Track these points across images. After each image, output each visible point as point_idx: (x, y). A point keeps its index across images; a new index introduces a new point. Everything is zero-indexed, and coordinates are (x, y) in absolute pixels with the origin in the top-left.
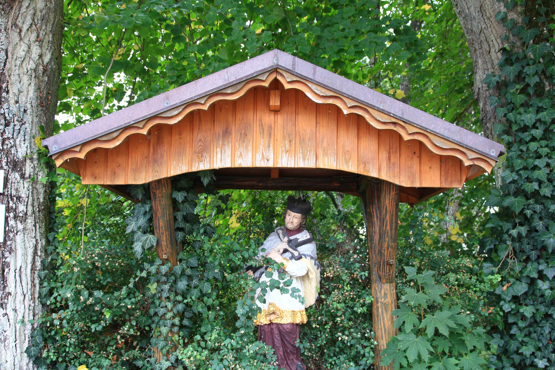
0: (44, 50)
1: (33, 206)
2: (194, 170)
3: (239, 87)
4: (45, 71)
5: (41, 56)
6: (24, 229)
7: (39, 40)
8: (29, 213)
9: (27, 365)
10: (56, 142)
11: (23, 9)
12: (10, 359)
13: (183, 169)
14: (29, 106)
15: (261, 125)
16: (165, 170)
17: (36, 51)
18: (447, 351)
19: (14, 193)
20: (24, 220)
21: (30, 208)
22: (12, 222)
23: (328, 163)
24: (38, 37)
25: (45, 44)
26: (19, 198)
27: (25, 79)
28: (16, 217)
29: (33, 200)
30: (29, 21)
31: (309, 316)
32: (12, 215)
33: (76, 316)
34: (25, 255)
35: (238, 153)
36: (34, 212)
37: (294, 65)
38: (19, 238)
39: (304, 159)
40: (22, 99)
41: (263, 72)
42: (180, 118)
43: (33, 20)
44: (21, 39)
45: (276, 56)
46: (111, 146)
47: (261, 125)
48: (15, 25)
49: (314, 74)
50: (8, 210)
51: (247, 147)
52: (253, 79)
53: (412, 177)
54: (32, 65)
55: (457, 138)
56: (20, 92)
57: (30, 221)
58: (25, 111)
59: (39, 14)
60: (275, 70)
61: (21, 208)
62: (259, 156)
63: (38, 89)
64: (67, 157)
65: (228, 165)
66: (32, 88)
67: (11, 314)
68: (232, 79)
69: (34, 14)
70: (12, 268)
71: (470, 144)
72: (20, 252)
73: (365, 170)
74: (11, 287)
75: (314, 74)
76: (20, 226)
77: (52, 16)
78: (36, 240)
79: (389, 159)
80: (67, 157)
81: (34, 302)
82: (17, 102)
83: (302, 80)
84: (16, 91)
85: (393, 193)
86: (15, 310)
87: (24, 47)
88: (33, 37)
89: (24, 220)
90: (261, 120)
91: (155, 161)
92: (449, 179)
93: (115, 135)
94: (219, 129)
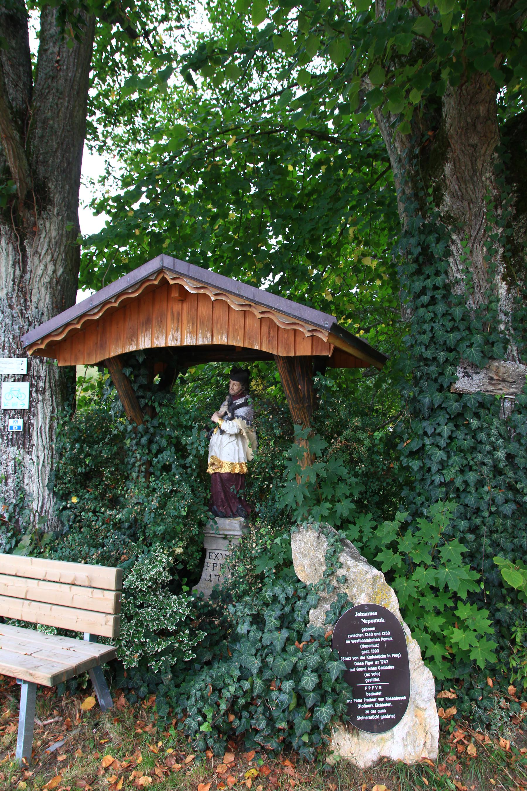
0: (57, 266)
1: (50, 382)
2: (126, 351)
3: (137, 287)
4: (57, 282)
5: (54, 272)
6: (44, 399)
7: (54, 261)
8: (47, 387)
9: (49, 495)
10: (27, 339)
11: (42, 240)
12: (35, 489)
13: (120, 351)
14: (45, 310)
15: (172, 313)
16: (107, 352)
17: (51, 268)
18: (329, 498)
19: (35, 374)
20: (43, 393)
21: (47, 384)
22: (34, 395)
23: (220, 340)
24: (53, 257)
25: (59, 262)
26: (39, 377)
27: (43, 290)
28: (37, 391)
29: (50, 378)
30: (46, 247)
31: (249, 468)
32: (34, 389)
33: (69, 462)
34: (44, 418)
35: (156, 336)
36: (50, 387)
37: (174, 265)
38: (40, 406)
39: (203, 338)
40: (41, 304)
41: (152, 274)
42: (100, 314)
43: (49, 246)
44: (40, 262)
45: (162, 260)
46: (59, 338)
47: (172, 313)
48: (36, 252)
49: (188, 270)
50: (31, 386)
51: (162, 331)
52: (146, 279)
53: (287, 348)
54: (47, 279)
55: (297, 314)
56: (39, 300)
57: (48, 394)
58: (43, 314)
59: (53, 240)
60: (160, 271)
61: (41, 384)
62: (170, 338)
63: (53, 295)
64: (35, 348)
65: (149, 346)
66: (48, 297)
67: (35, 459)
68: (133, 282)
69: (50, 242)
70: (35, 427)
71: (308, 318)
72: (40, 416)
73: (249, 344)
74: (35, 441)
75: (188, 270)
76: (40, 398)
77: (64, 240)
78: (53, 408)
79: (269, 333)
80: (35, 348)
81: (52, 452)
82: (37, 308)
83: (180, 275)
84: (36, 300)
85: (281, 362)
86: (38, 457)
87: (42, 267)
88: (49, 258)
89: (43, 393)
90: (172, 309)
91: (101, 346)
92: (320, 348)
93: (60, 330)
94: (143, 318)
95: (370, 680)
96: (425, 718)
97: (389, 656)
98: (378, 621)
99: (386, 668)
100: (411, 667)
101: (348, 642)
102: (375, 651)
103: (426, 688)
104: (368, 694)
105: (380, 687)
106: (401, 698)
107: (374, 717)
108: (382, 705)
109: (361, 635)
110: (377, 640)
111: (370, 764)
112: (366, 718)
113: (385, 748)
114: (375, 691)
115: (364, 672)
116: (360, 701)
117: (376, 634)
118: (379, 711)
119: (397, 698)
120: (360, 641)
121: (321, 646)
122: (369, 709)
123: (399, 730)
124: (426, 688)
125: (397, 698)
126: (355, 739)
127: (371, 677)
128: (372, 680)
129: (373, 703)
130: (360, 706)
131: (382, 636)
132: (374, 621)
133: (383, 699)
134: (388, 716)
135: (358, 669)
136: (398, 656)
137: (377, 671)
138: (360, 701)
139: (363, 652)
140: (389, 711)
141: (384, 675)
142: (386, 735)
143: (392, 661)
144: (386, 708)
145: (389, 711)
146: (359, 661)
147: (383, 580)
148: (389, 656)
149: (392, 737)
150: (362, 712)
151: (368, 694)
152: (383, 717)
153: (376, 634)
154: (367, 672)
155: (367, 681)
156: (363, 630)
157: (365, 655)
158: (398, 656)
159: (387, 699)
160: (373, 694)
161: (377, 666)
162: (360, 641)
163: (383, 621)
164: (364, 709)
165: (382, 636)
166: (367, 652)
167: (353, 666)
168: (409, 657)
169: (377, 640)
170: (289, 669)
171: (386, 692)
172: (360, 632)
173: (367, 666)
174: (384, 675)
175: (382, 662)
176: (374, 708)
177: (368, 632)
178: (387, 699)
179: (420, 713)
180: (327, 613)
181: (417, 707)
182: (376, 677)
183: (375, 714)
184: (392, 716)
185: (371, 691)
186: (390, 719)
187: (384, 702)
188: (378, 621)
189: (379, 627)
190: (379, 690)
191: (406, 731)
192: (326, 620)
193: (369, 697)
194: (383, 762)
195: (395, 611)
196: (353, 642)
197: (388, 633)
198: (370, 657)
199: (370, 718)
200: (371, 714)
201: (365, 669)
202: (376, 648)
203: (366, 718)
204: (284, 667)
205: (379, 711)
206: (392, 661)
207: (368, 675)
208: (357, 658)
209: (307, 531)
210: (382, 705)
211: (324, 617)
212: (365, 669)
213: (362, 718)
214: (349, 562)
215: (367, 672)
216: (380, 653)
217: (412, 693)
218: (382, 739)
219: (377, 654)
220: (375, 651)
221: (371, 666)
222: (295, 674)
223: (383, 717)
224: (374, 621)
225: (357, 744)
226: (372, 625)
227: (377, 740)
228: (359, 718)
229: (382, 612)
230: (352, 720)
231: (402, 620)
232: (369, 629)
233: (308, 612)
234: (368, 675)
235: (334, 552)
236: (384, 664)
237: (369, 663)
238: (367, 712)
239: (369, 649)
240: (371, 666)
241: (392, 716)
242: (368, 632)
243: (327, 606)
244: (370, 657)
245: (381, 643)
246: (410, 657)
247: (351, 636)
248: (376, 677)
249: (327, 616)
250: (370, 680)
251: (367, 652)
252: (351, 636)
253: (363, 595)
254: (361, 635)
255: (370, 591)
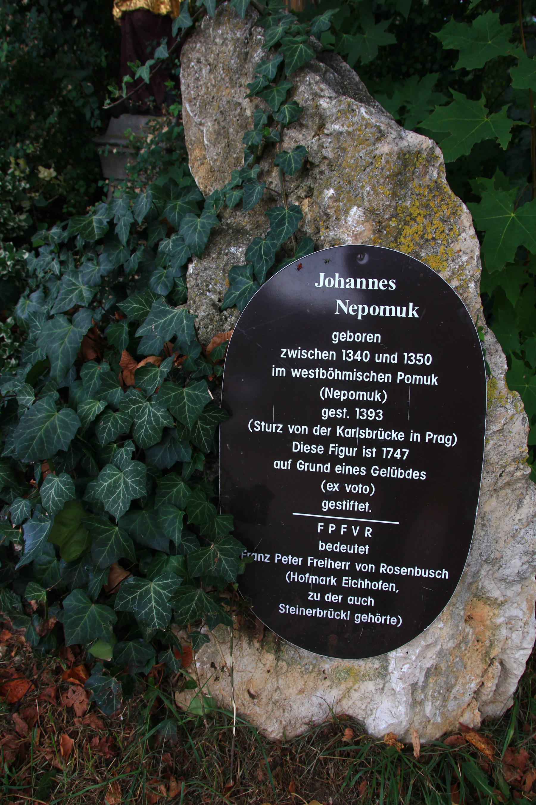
95: (339, 505)
96: (497, 627)
97: (415, 437)
98: (397, 312)
99: (399, 473)
100: (486, 481)
101: (279, 371)
102: (371, 414)
103: (520, 548)
104: (322, 546)
105: (368, 532)
106: (432, 574)
107: (333, 615)
108: (365, 584)
109: (332, 355)
110: (386, 377)
111: (302, 729)
112: (309, 612)
113: (355, 695)
114: (348, 539)
115: (321, 476)
116: (297, 561)
117: (379, 359)
118: (352, 600)
119: (417, 572)
120: (321, 373)
121: (178, 377)
122: (323, 589)
123: (405, 663)
124: (520, 548)
125: (417, 572)
126: (270, 658)
127: (341, 495)
128: (345, 506)
129: (339, 574)
130: (293, 577)
131: (401, 366)
132: (380, 311)
133: (370, 568)
134: (378, 619)
135: (302, 466)
136: (448, 441)
137: (367, 480)
138: (297, 561)
139: (327, 413)
140: (384, 603)
141: (389, 497)
142: (368, 665)
143: (420, 455)
144: (376, 594)
145: (384, 603)
146: (310, 439)
147: (437, 173)
148: (415, 437)
149: (383, 673)
150: (298, 594)
151: (322, 546)
152: (360, 618)
153: (379, 359)
154: (332, 477)
155: (327, 505)
156: (337, 337)
157: (333, 423)
158: (448, 441)
159: (383, 568)
160: (342, 548)
161: (368, 463)
162: (321, 373)
163: (413, 313)
164: (307, 587)
165: (401, 366)
166: (342, 413)
167: (286, 454)
168: (488, 447)
169: (386, 377)
170: (63, 438)
171: (384, 548)
172: (327, 346)
173: (335, 460)
174: (389, 497)
175: (388, 452)
176: (337, 589)
177: (355, 346)
178: (383, 568)
179: (483, 611)
180: (233, 272)
181: (480, 596)
182: (360, 498)
183: (336, 607)
184: (393, 621)
185: (335, 538)
186: (385, 626)
187: (375, 576)
188: (397, 312)
189: (396, 335)
190: (361, 540)
191: (428, 663)
192: (229, 294)
193: (324, 555)
194: (340, 732)
195: (464, 287)
196: (295, 373)
197: (427, 360)
198: (350, 433)
199: (320, 613)
200: (323, 605)
201: (326, 468)
202: (375, 405)
203: (309, 612)
204: (50, 432)
205: (352, 600)
206: (420, 455)
207: (333, 487)
208: (303, 429)
209: (218, 24)
210: (365, 584)
211: (222, 287)
212: (326, 468)
213: (292, 610)
214: (324, 103)
215: (332, 477)
216: (386, 425)
217: (472, 558)
218: (348, 671)
219: (373, 425)
220: (371, 414)
221: (348, 461)
222: (85, 455)
223: (360, 618)
224: (380, 311)
225: (274, 672)
226: (370, 324)
227: (336, 670)
228: (284, 608)
229: (418, 282)
230: (261, 609)
231: (482, 322)
232: (360, 337)
233: (185, 268)
234: (333, 487)
235: (281, 67)
236: (393, 462)
237: (342, 452)
238: (313, 596)
239: (351, 405)
240: (348, 461)
241: (393, 621)
242: (355, 346)
243: (238, 252)
244: (350, 433)
245: (395, 389)
246: (490, 447)
247: (292, 354)
248: (360, 498)
249: (233, 282)
250: (339, 505)
251: (342, 413)
252: (292, 354)
253: (355, 212)
254: (325, 355)
255: (383, 199)
